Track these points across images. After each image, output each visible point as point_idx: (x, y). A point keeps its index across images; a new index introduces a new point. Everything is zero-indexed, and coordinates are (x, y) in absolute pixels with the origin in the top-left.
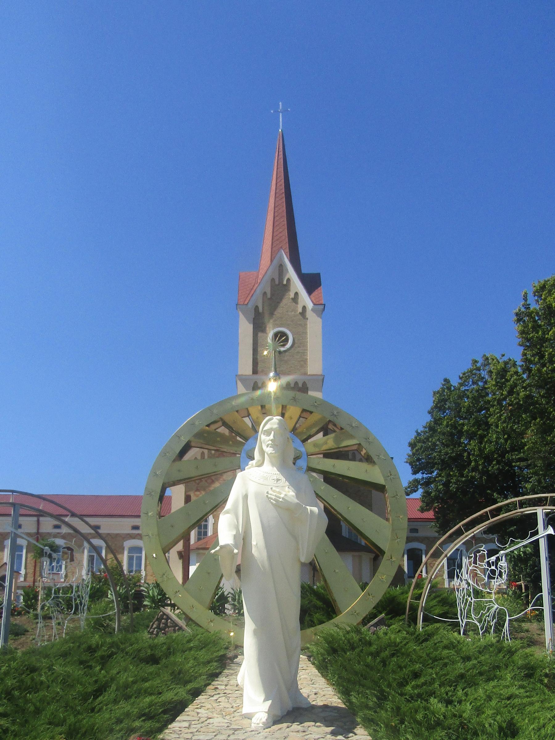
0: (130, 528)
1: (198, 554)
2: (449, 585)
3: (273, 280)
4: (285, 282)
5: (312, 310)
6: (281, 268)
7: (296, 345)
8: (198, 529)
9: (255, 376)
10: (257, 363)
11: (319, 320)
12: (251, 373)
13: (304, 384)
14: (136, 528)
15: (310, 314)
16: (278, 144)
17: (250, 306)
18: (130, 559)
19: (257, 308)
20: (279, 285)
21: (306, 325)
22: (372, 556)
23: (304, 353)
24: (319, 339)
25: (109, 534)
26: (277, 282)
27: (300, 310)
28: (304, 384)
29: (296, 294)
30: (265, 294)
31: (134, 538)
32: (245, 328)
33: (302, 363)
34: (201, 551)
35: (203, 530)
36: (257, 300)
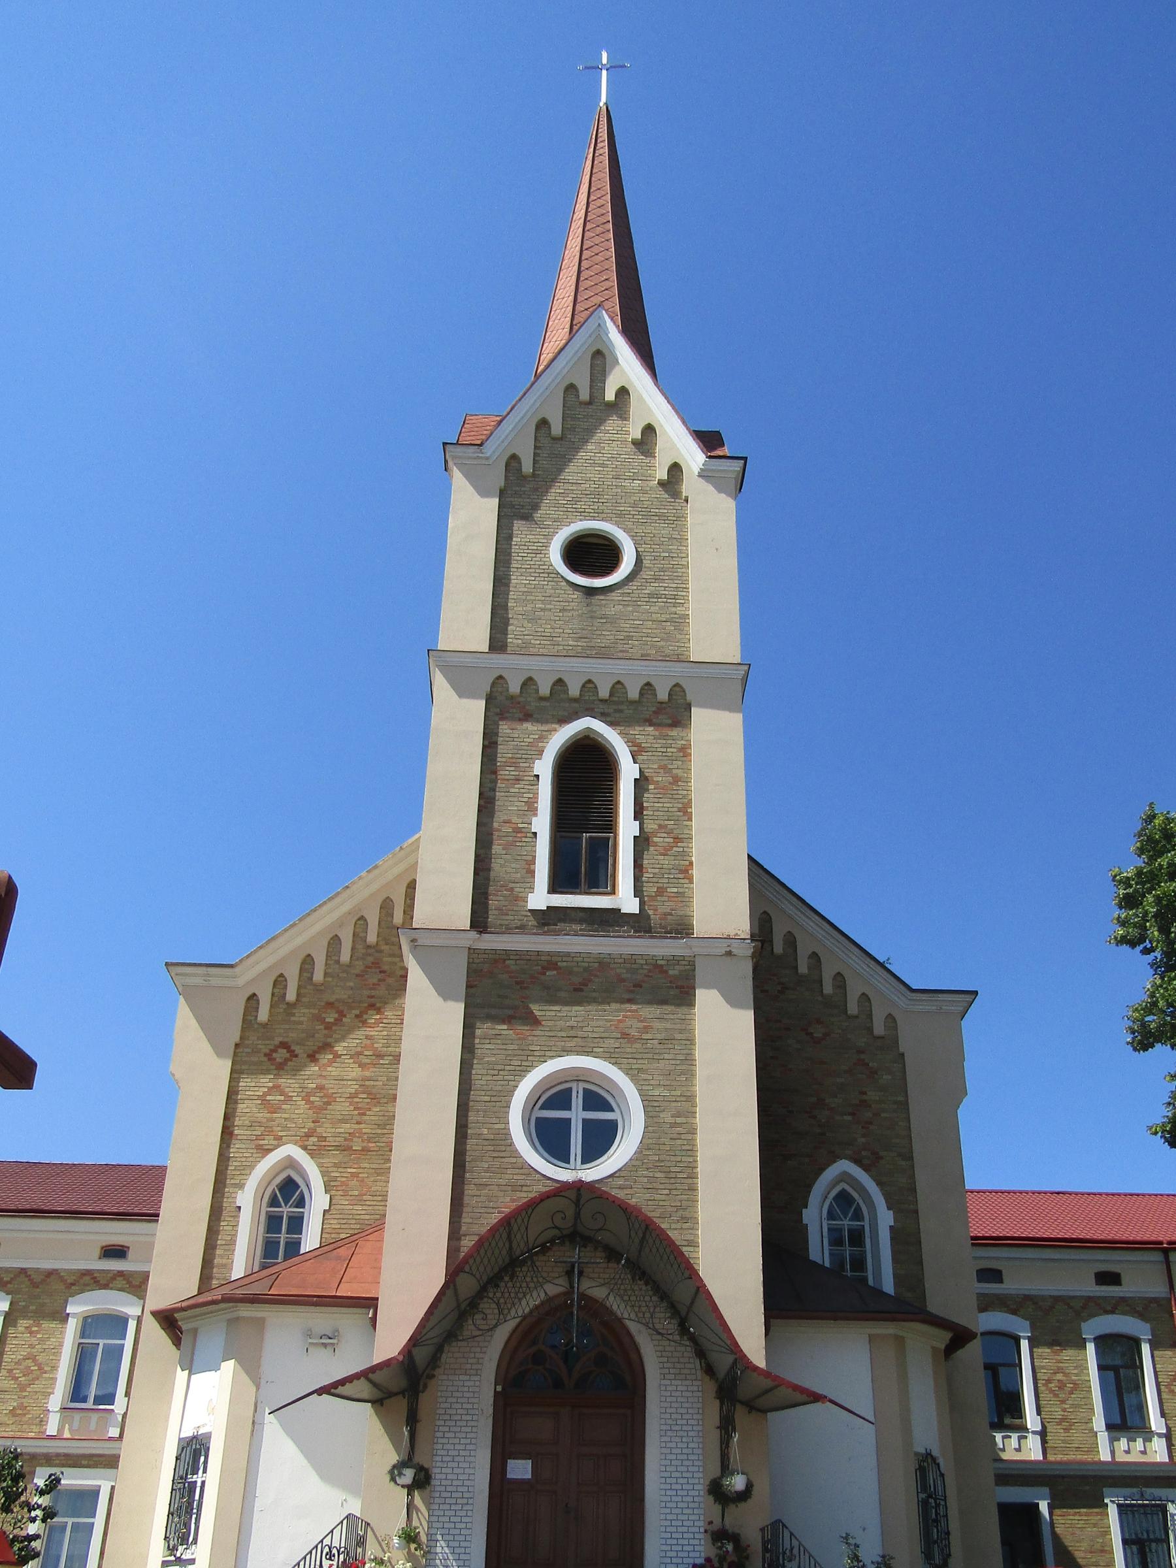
0: (97, 1252)
1: (233, 1322)
2: (1113, 1453)
3: (571, 388)
4: (610, 396)
5: (703, 475)
6: (600, 360)
7: (645, 574)
8: (298, 1244)
9: (499, 659)
10: (506, 622)
11: (726, 505)
12: (485, 647)
13: (677, 690)
14: (115, 1252)
15: (691, 484)
16: (590, 175)
17: (490, 449)
18: (84, 1356)
19: (513, 461)
20: (590, 403)
21: (680, 518)
22: (942, 1338)
23: (677, 596)
24: (729, 562)
25: (23, 1271)
26: (584, 395)
27: (662, 474)
28: (677, 690)
29: (649, 430)
30: (543, 424)
31: (106, 1287)
32: (472, 515)
33: (670, 627)
34: (246, 1311)
35: (283, 1237)
36: (513, 437)
